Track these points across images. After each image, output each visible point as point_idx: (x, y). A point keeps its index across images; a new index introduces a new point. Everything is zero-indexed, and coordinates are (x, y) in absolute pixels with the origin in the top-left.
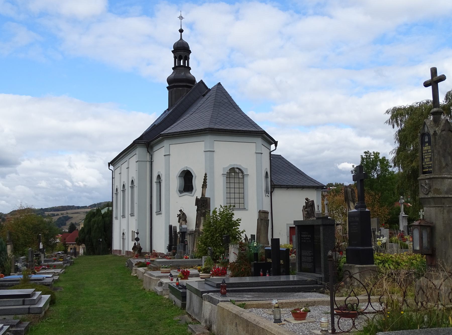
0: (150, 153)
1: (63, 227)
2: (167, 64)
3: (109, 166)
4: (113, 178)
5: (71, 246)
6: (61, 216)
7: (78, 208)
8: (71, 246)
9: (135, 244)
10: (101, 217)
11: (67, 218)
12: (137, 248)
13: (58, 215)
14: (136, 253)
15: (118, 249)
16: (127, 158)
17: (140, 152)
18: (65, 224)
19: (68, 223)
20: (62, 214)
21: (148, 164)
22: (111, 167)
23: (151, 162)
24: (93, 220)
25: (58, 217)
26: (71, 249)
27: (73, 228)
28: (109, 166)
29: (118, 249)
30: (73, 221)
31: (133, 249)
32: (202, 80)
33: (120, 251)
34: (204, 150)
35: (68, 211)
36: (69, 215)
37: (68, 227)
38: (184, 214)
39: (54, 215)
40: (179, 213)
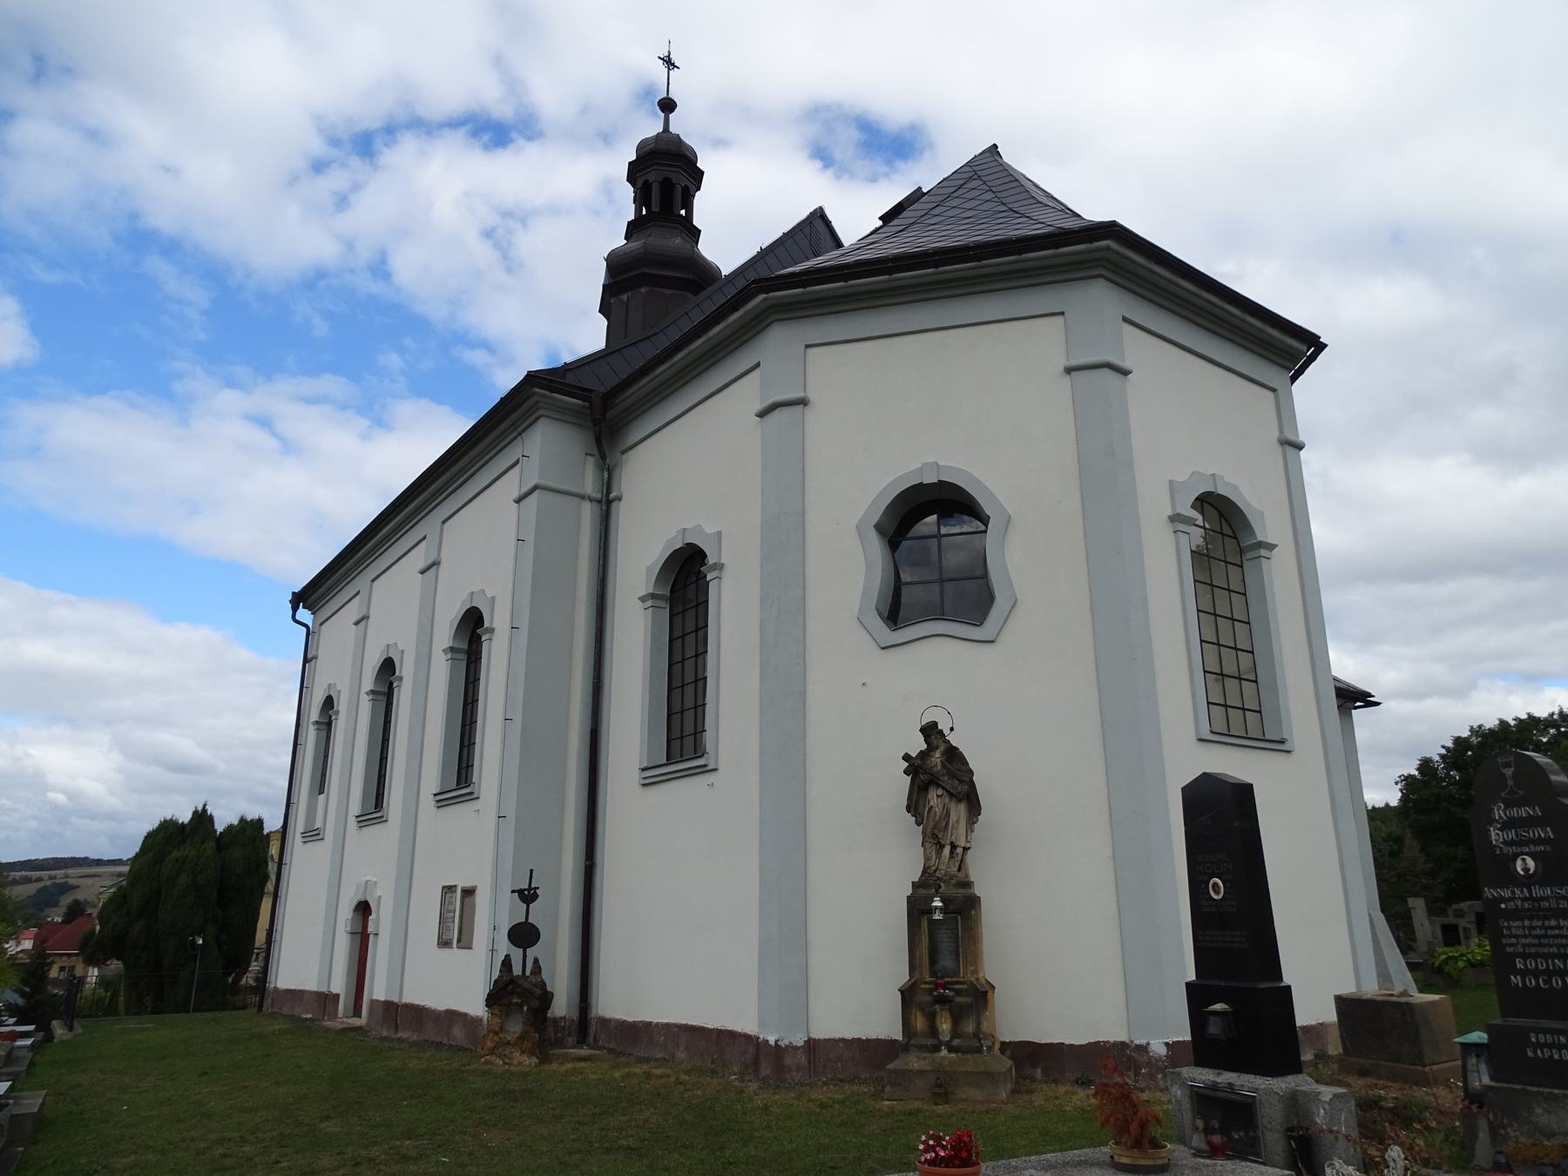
0: (603, 456)
1: (48, 911)
2: (605, 217)
3: (295, 609)
4: (306, 660)
5: (64, 962)
6: (49, 883)
7: (99, 862)
8: (64, 962)
9: (507, 963)
10: (210, 846)
11: (65, 888)
12: (514, 992)
13: (39, 879)
14: (515, 1027)
15: (311, 986)
16: (428, 525)
17: (546, 448)
18: (56, 904)
19: (66, 900)
20: (51, 878)
21: (588, 512)
22: (304, 614)
23: (606, 504)
24: (175, 854)
25: (40, 885)
26: (62, 969)
27: (76, 911)
28: (295, 609)
29: (311, 984)
30: (80, 896)
31: (492, 1000)
32: (821, 208)
33: (326, 1001)
34: (1062, 363)
35: (70, 871)
36: (72, 882)
37: (63, 910)
38: (953, 754)
39: (28, 880)
40: (917, 745)
